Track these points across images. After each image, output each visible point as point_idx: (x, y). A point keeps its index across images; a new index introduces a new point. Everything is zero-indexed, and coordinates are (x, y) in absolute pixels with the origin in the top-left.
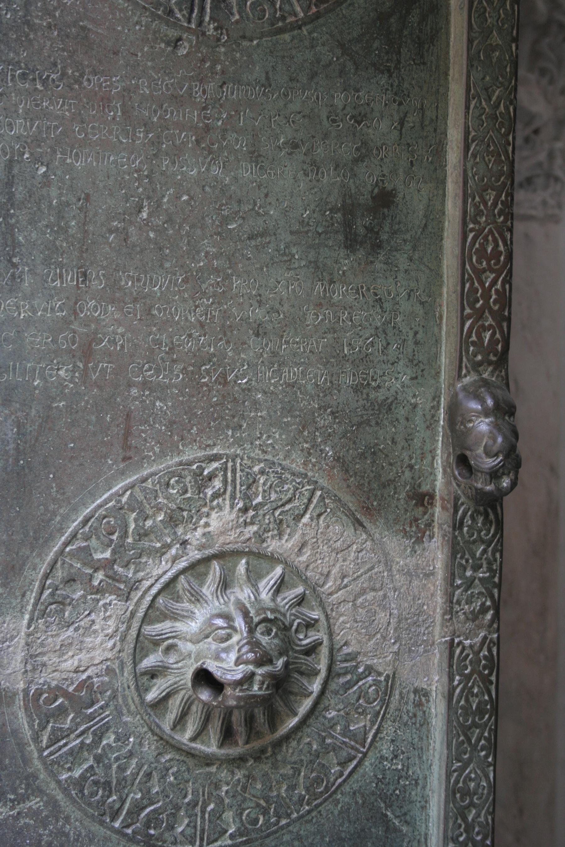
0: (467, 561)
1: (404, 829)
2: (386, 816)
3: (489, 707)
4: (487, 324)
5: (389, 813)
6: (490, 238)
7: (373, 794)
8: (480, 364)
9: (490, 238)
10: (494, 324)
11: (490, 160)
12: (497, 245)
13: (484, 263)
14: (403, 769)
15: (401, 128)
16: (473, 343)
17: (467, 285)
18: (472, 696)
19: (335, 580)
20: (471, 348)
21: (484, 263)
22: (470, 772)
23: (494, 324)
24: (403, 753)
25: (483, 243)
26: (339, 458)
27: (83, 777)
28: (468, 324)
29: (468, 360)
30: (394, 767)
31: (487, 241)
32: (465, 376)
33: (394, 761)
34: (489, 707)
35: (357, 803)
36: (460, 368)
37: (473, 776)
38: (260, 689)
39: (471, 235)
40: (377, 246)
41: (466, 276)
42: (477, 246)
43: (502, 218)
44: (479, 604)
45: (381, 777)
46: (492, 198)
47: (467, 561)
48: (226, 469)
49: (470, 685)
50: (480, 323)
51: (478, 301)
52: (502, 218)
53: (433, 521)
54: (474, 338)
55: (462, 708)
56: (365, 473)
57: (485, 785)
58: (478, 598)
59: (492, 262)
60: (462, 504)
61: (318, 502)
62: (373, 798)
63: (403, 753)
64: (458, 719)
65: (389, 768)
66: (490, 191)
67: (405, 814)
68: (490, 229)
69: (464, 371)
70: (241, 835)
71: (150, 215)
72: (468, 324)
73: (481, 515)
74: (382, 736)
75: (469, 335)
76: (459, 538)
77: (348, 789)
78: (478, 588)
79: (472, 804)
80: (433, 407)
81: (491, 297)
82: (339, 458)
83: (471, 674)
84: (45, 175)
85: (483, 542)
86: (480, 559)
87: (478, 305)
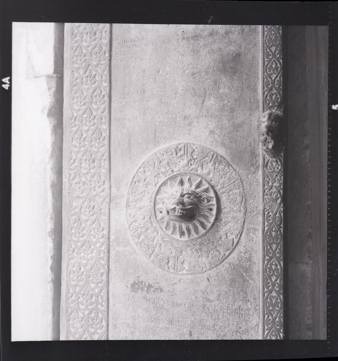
0: (269, 179)
1: (251, 282)
2: (243, 275)
3: (279, 237)
4: (273, 93)
5: (244, 274)
6: (274, 63)
7: (237, 265)
8: (272, 107)
9: (274, 63)
10: (276, 92)
11: (272, 37)
12: (277, 64)
13: (272, 72)
14: (249, 258)
15: (242, 33)
16: (268, 100)
17: (265, 80)
18: (273, 231)
19: (221, 185)
20: (267, 101)
21: (272, 72)
22: (273, 262)
23: (276, 92)
24: (249, 251)
25: (271, 65)
26: (223, 143)
27: (141, 242)
28: (266, 93)
29: (266, 105)
30: (246, 256)
31: (273, 64)
32: (266, 111)
33: (246, 254)
34: (279, 237)
35: (231, 267)
36: (264, 109)
37: (274, 263)
38: (178, 213)
39: (266, 63)
40: (235, 73)
41: (265, 77)
42: (269, 66)
43: (278, 56)
44: (275, 195)
45: (240, 259)
46: (274, 49)
47: (269, 179)
48: (185, 147)
49: (272, 227)
50: (271, 92)
51: (270, 85)
52: (278, 56)
53: (259, 165)
54: (268, 98)
55: (268, 235)
56: (233, 148)
57: (279, 268)
58: (274, 193)
59: (275, 71)
60: (267, 158)
61: (215, 158)
62: (237, 267)
63: (249, 251)
64: (267, 239)
65: (243, 257)
66: (273, 47)
67: (250, 276)
68: (274, 60)
69: (265, 109)
70: (189, 271)
71: (162, 73)
72: (266, 93)
73: (275, 162)
74: (241, 244)
75: (267, 97)
76: (266, 171)
77: (227, 261)
78: (274, 190)
79: (273, 274)
80: (258, 124)
81: (275, 83)
82: (223, 143)
83: (272, 223)
84: (134, 66)
85: (276, 172)
86: (275, 179)
87: (270, 86)
